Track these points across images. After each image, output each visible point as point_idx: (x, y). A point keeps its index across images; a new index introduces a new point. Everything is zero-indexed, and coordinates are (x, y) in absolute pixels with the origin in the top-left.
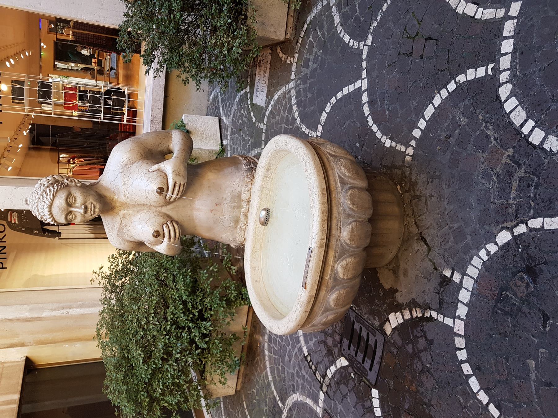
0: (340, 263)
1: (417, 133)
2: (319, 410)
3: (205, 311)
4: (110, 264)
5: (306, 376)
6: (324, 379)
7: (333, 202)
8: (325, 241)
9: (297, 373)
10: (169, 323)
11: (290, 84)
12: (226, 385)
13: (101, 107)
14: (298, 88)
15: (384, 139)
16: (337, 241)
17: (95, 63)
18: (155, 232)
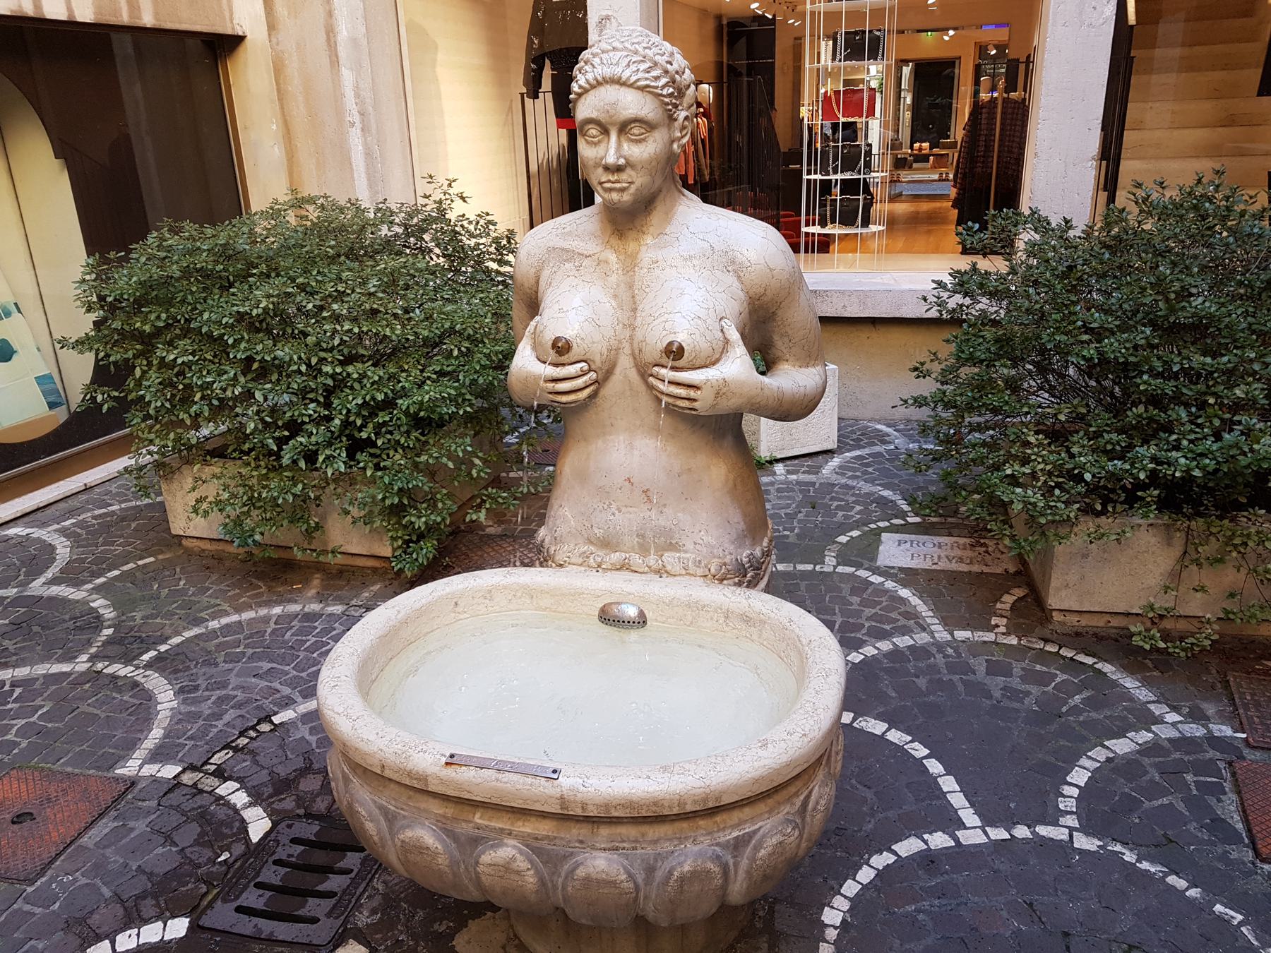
0: (521, 852)
2: (130, 768)
3: (372, 455)
4: (472, 218)
5: (220, 724)
6: (213, 774)
7: (685, 825)
8: (579, 812)
9: (227, 698)
10: (338, 370)
11: (940, 628)
12: (194, 515)
13: (835, 172)
14: (934, 650)
15: (841, 903)
16: (581, 842)
17: (920, 149)
18: (567, 342)
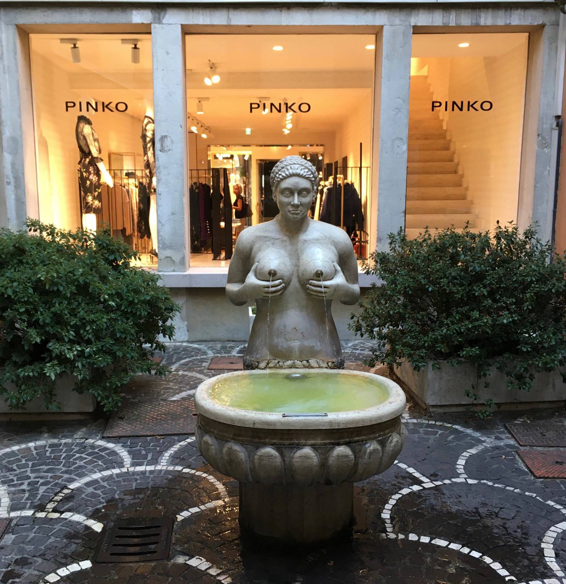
1: (413, 537)
18: (275, 271)
